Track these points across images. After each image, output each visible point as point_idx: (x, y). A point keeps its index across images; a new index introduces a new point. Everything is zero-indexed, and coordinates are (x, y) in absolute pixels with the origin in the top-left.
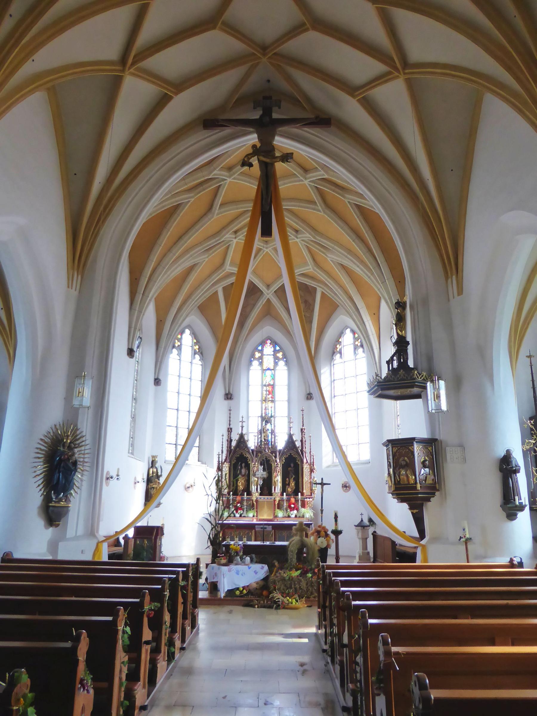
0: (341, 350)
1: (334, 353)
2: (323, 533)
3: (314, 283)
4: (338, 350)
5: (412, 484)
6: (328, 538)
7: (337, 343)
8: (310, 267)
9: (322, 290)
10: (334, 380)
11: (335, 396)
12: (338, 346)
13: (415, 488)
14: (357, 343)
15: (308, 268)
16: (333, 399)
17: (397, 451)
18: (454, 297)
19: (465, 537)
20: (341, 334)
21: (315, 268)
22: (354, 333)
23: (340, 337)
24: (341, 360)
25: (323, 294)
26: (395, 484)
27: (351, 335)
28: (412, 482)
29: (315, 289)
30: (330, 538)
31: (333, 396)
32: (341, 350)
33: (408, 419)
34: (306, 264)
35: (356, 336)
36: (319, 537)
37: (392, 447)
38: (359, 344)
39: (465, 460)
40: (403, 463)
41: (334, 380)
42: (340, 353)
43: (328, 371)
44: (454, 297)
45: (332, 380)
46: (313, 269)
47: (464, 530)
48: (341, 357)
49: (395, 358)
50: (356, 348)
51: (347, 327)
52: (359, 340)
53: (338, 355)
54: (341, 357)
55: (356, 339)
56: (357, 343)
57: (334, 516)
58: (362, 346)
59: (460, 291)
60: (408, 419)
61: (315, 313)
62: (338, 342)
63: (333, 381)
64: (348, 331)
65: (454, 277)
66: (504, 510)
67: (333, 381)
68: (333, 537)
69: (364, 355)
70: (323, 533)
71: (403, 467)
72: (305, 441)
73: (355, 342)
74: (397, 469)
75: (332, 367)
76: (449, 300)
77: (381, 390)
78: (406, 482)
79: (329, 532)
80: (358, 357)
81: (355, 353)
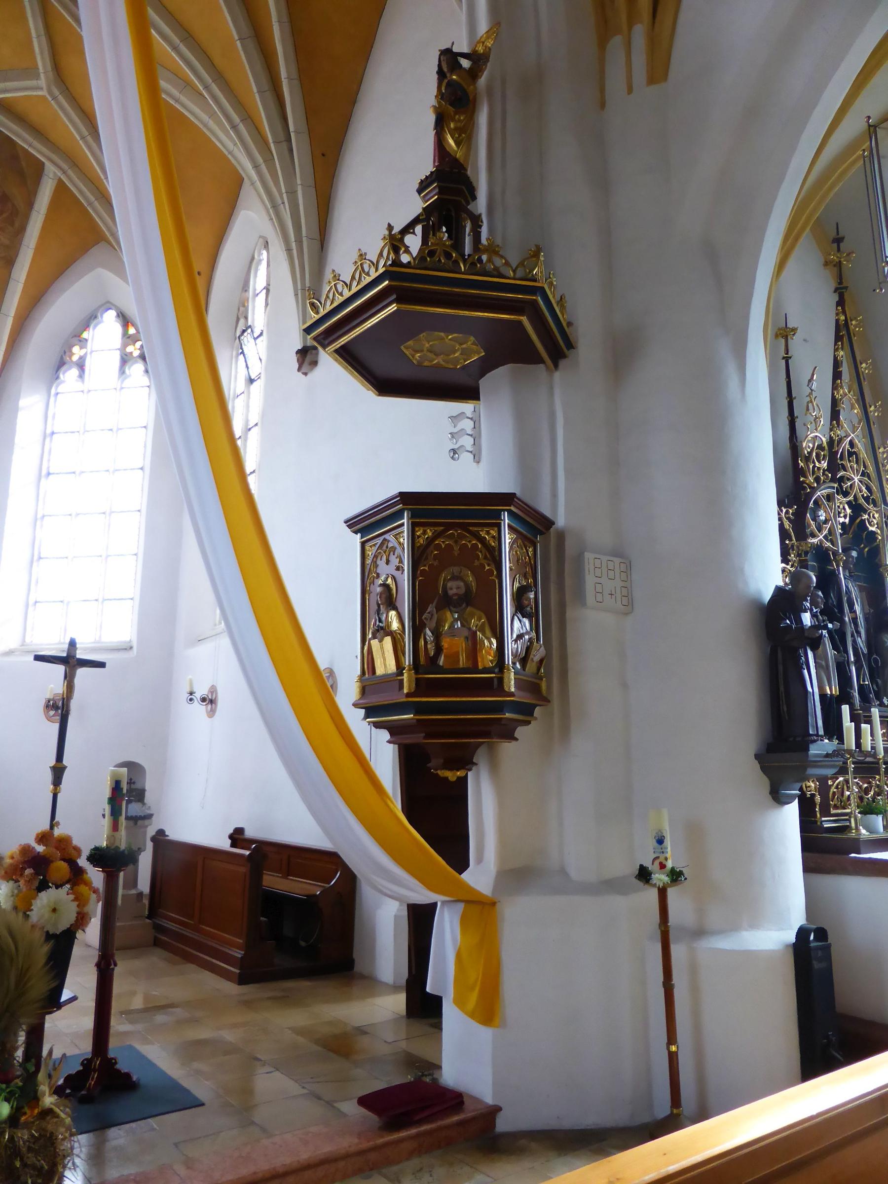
0: (82, 359)
1: (61, 364)
2: (61, 868)
3: (44, 150)
4: (75, 358)
5: (486, 670)
6: (83, 889)
7: (75, 340)
8: (42, 82)
9: (59, 174)
10: (53, 433)
11: (49, 474)
12: (76, 349)
13: (496, 686)
14: (130, 349)
15: (33, 83)
16: (43, 480)
17: (430, 541)
18: (630, 90)
19: (662, 866)
20: (90, 320)
21: (56, 92)
22: (125, 320)
23: (86, 327)
24: (79, 385)
25: (61, 188)
26: (416, 666)
27: (118, 328)
28: (487, 658)
29: (39, 168)
30: (88, 884)
31: (44, 472)
32: (82, 359)
33: (433, 447)
34: (31, 72)
35: (132, 331)
36: (43, 886)
37: (414, 526)
38: (136, 353)
39: (629, 606)
40: (455, 588)
41: (53, 433)
42: (81, 366)
43: (41, 406)
44: (630, 90)
45: (48, 431)
46: (50, 92)
47: (660, 841)
48: (81, 376)
49: (419, 229)
50: (125, 360)
51: (108, 305)
52: (138, 344)
53: (74, 372)
54: (81, 376)
55: (128, 339)
56: (130, 349)
57: (107, 793)
58: (143, 357)
59: (659, 69)
60: (433, 447)
61: (25, 241)
62: (76, 337)
63: (48, 435)
64: (110, 316)
65: (639, 33)
66: (764, 769)
67: (48, 435)
68: (96, 876)
69: (145, 381)
70: (61, 868)
71: (447, 602)
72: (54, 417)
73: (125, 346)
74: (431, 608)
75: (52, 399)
76: (603, 105)
77: (398, 301)
78: (463, 662)
79: (83, 862)
80: (127, 383)
81: (122, 372)
